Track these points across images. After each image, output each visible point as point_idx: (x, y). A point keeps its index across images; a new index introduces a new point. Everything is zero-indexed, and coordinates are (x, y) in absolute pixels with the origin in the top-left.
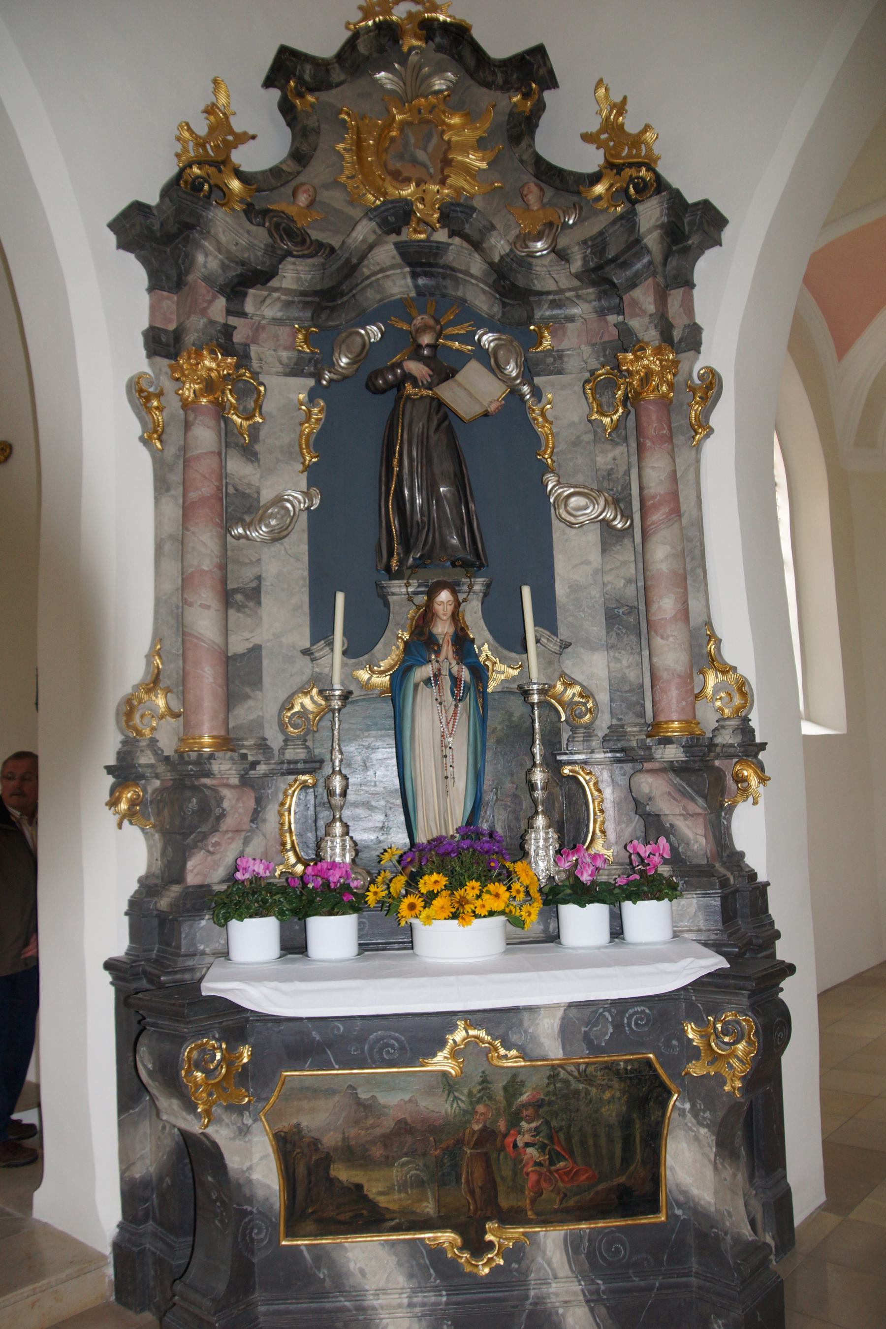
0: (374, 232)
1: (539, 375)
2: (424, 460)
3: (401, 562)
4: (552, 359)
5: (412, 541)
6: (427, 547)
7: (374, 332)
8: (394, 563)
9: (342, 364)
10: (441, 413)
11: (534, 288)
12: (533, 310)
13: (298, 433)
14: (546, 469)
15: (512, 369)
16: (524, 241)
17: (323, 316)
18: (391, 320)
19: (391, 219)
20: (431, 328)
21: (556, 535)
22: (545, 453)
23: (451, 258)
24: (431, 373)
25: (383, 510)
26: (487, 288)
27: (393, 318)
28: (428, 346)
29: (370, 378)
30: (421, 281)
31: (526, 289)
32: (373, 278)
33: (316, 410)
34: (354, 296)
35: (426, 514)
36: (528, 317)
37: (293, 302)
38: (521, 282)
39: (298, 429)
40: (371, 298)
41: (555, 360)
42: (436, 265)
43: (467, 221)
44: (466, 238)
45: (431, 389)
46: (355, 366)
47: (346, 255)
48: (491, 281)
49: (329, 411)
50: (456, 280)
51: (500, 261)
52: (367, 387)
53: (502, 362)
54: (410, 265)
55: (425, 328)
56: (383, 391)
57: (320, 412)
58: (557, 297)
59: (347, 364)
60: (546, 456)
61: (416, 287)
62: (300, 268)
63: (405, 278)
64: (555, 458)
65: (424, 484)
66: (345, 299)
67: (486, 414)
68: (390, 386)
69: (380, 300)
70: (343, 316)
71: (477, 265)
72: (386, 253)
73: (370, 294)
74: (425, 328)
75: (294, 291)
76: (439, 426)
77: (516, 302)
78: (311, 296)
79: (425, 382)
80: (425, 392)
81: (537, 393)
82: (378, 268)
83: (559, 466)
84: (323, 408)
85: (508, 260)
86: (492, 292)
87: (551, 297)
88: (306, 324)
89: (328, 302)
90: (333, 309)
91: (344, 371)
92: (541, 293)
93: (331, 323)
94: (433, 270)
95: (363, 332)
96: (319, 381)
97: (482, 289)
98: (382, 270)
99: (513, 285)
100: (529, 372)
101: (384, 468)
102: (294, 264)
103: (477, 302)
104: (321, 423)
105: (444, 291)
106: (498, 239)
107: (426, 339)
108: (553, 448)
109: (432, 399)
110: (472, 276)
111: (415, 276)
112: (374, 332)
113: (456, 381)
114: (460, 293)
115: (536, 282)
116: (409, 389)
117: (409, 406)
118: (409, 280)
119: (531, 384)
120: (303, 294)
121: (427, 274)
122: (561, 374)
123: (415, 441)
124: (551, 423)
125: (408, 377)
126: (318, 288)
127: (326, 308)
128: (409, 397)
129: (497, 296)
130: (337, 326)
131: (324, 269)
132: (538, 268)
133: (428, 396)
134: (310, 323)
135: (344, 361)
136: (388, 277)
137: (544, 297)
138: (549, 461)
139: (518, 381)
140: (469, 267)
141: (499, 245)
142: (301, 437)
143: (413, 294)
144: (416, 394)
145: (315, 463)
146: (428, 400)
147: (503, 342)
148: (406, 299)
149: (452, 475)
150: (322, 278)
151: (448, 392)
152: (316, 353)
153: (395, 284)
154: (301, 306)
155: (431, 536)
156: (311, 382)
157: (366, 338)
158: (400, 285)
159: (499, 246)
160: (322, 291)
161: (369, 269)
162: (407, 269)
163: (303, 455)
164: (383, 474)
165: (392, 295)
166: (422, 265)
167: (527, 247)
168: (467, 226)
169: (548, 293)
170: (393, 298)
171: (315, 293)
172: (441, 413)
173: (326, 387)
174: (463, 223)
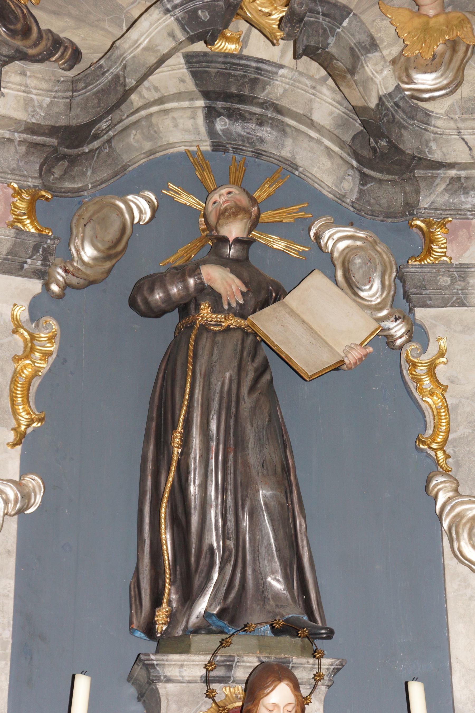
0: (172, 35)
1: (426, 306)
2: (232, 440)
3: (173, 618)
4: (449, 280)
5: (197, 582)
6: (232, 595)
7: (140, 206)
8: (161, 617)
9: (86, 259)
10: (259, 360)
11: (430, 157)
12: (418, 192)
13: (10, 375)
14: (435, 468)
15: (373, 292)
16: (407, 70)
17: (57, 172)
18: (169, 189)
19: (204, 15)
20: (246, 211)
21: (452, 587)
22: (433, 441)
23: (280, 91)
24: (244, 289)
25: (147, 520)
26: (336, 149)
27: (171, 186)
28: (237, 241)
29: (138, 288)
30: (220, 125)
31: (414, 157)
32: (143, 113)
33: (43, 335)
34: (109, 141)
35: (232, 535)
36: (407, 204)
37: (10, 140)
38: (409, 144)
39: (10, 368)
40: (135, 147)
41: (453, 282)
42: (251, 101)
43: (332, 31)
44: (325, 61)
45: (244, 317)
46: (108, 265)
47: (115, 70)
48: (347, 138)
49: (66, 338)
50: (282, 128)
51: (377, 105)
52: (133, 303)
53: (357, 276)
54: (206, 95)
55: (235, 211)
56: (156, 313)
57: (50, 339)
58: (463, 173)
59: (95, 259)
60: (434, 446)
61: (212, 132)
62: (32, 83)
63: (194, 117)
64: (449, 450)
65: (230, 482)
66: (96, 144)
67: (338, 367)
68: (170, 305)
69: (152, 152)
70: (89, 173)
71: (325, 105)
72: (174, 76)
73: (134, 137)
74: (235, 211)
75: (18, 122)
76: (256, 380)
77: (386, 177)
78: (43, 134)
79: (234, 305)
80: (233, 322)
81: (417, 333)
82: (156, 96)
83: (458, 464)
84: (54, 337)
85: (389, 105)
86: (345, 155)
87: (453, 173)
88: (30, 183)
89: (68, 147)
90: (73, 161)
91: (88, 272)
92: (439, 165)
93: (68, 185)
94: (245, 107)
95: (122, 206)
96: (46, 286)
97: (327, 148)
98: (161, 101)
99: (394, 148)
100: (407, 296)
101: (152, 447)
102: (23, 74)
103: (315, 171)
104: (51, 360)
105: (258, 146)
106: (379, 68)
107: (234, 230)
108: (448, 432)
109: (245, 333)
110: (312, 124)
111: (211, 114)
112: (140, 206)
113: (286, 306)
114: (285, 153)
115: (434, 147)
116: (205, 311)
117: (205, 342)
118: (200, 120)
119: (406, 316)
120: (32, 129)
121: (233, 115)
122: (464, 305)
123: (215, 404)
124: (445, 389)
125: (206, 292)
126: (62, 122)
127: (64, 157)
128: (204, 328)
129: (354, 163)
130: (79, 190)
131: (73, 91)
132: (439, 123)
133: (238, 328)
134: (37, 182)
135: (89, 253)
136: (166, 112)
137: (441, 172)
138: (440, 454)
139: (384, 313)
140: (311, 110)
141: (379, 78)
142: (14, 381)
143: (206, 147)
144: (218, 324)
145: (35, 429)
146: (238, 335)
147: (359, 243)
148: (193, 154)
149: (279, 469)
150: (70, 107)
151: (268, 322)
152: (47, 236)
153: (176, 126)
154: (23, 149)
155: (238, 575)
156: (36, 286)
157: (127, 216)
158: (183, 127)
159: (378, 79)
160: (67, 128)
161: (141, 96)
162: (201, 103)
163: (15, 413)
164: (150, 456)
165: (171, 145)
166: (228, 97)
167: (411, 81)
168: (331, 40)
169: (451, 166)
170: (171, 151)
171: (53, 131)
172: (259, 360)
173: (60, 297)
174: (325, 35)
